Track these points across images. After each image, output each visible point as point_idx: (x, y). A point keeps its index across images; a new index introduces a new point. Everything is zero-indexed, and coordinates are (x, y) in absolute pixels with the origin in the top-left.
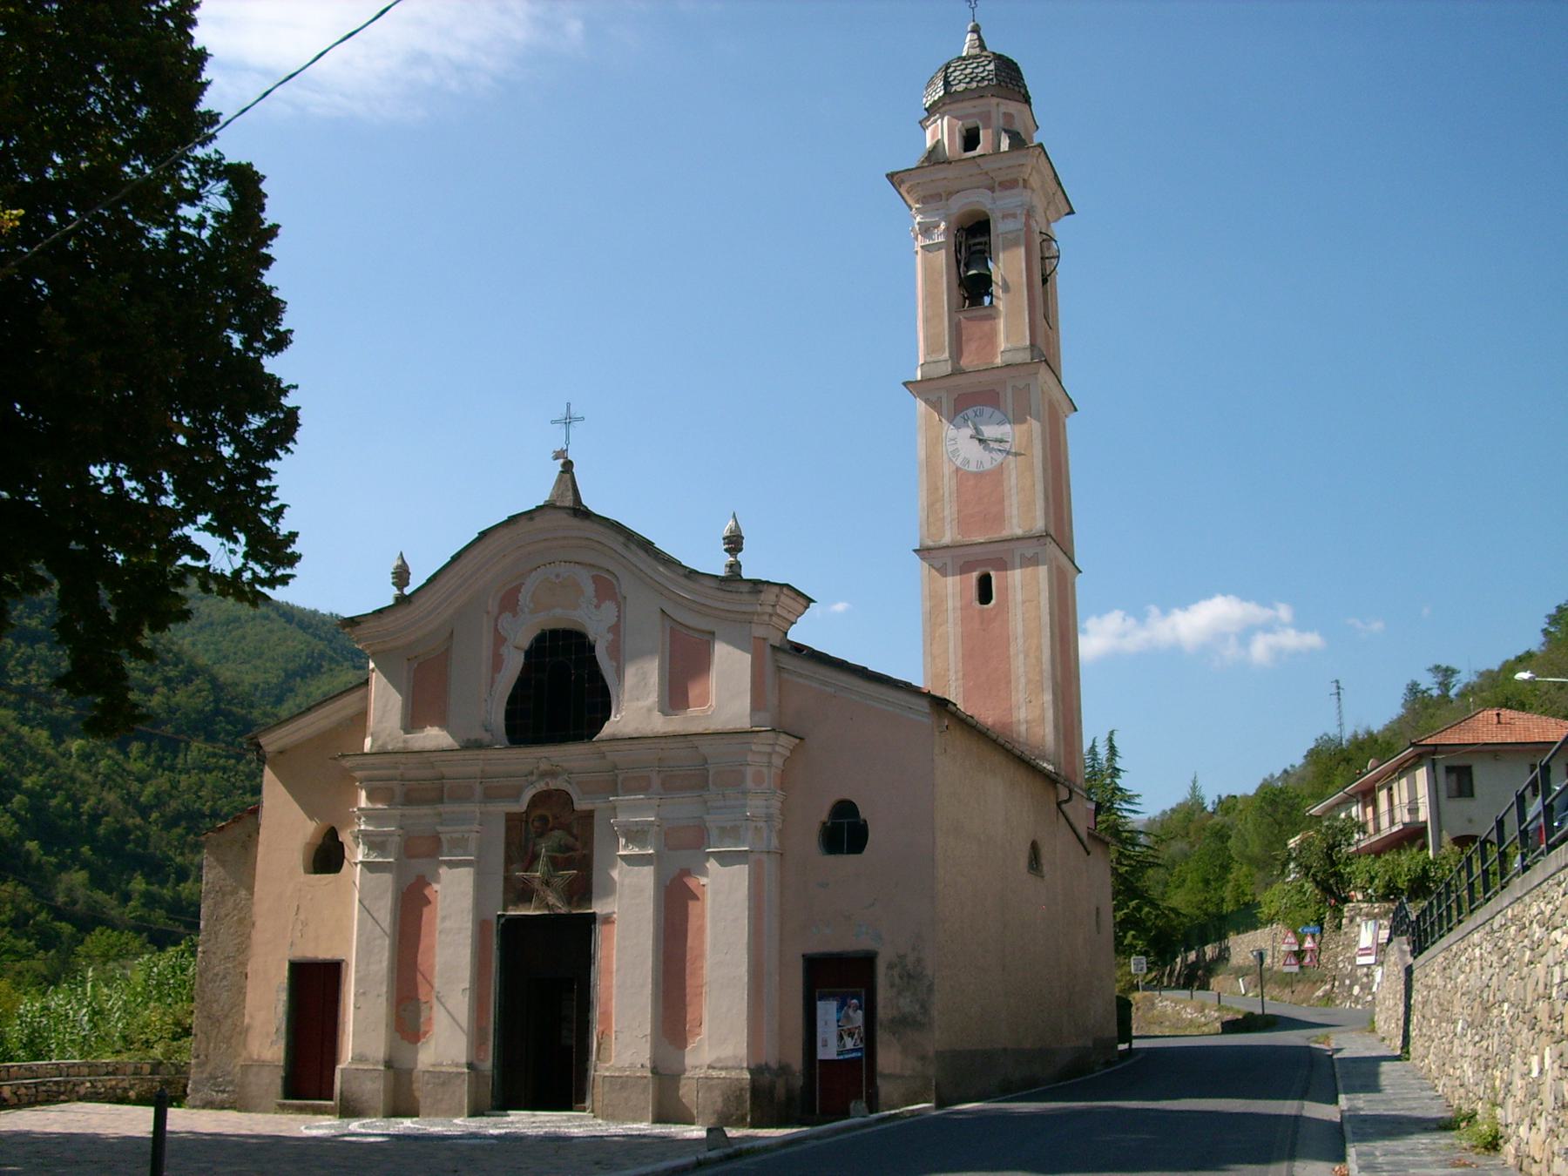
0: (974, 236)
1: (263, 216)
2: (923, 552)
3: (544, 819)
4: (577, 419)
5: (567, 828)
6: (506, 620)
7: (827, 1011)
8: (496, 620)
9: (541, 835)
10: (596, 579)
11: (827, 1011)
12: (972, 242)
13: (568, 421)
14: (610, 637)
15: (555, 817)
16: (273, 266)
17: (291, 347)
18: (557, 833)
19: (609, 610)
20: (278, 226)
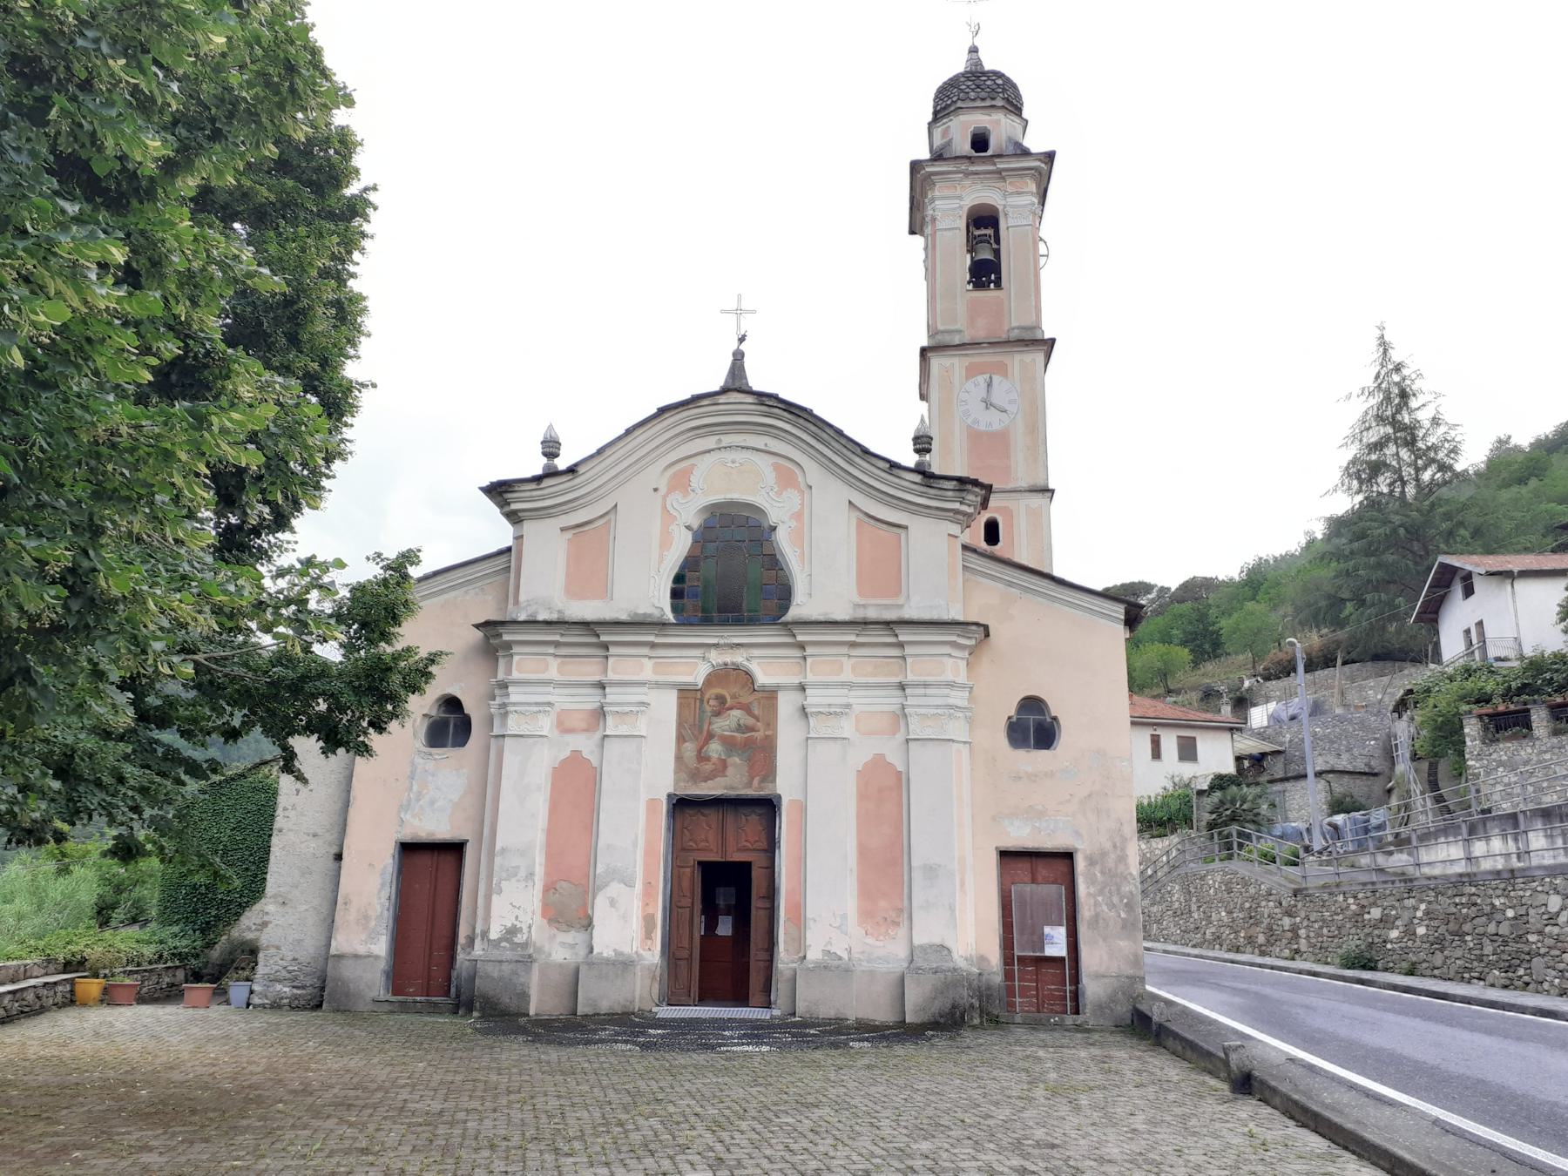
0: (978, 228)
1: (321, 743)
2: (1048, 492)
3: (721, 699)
4: (739, 301)
5: (747, 709)
6: (676, 499)
7: (1056, 946)
8: (665, 498)
9: (718, 714)
10: (776, 467)
11: (1056, 946)
12: (977, 233)
13: (739, 312)
14: (793, 524)
15: (734, 697)
16: (433, 682)
17: (375, 224)
18: (736, 713)
19: (792, 498)
20: (482, 489)
